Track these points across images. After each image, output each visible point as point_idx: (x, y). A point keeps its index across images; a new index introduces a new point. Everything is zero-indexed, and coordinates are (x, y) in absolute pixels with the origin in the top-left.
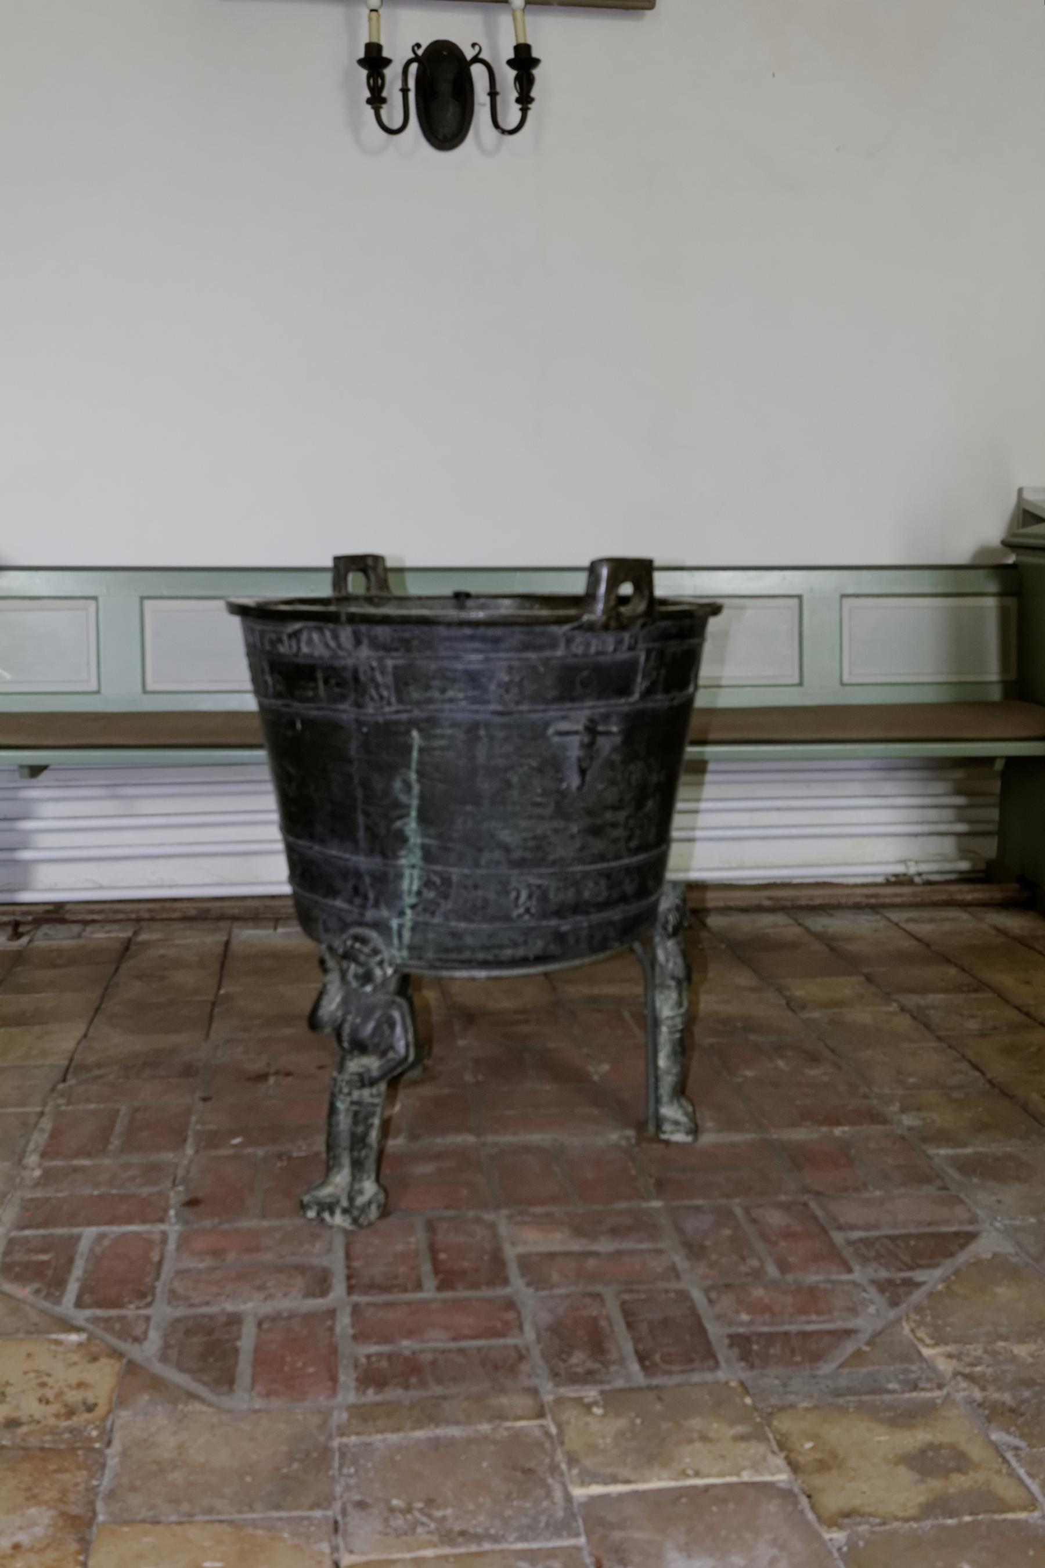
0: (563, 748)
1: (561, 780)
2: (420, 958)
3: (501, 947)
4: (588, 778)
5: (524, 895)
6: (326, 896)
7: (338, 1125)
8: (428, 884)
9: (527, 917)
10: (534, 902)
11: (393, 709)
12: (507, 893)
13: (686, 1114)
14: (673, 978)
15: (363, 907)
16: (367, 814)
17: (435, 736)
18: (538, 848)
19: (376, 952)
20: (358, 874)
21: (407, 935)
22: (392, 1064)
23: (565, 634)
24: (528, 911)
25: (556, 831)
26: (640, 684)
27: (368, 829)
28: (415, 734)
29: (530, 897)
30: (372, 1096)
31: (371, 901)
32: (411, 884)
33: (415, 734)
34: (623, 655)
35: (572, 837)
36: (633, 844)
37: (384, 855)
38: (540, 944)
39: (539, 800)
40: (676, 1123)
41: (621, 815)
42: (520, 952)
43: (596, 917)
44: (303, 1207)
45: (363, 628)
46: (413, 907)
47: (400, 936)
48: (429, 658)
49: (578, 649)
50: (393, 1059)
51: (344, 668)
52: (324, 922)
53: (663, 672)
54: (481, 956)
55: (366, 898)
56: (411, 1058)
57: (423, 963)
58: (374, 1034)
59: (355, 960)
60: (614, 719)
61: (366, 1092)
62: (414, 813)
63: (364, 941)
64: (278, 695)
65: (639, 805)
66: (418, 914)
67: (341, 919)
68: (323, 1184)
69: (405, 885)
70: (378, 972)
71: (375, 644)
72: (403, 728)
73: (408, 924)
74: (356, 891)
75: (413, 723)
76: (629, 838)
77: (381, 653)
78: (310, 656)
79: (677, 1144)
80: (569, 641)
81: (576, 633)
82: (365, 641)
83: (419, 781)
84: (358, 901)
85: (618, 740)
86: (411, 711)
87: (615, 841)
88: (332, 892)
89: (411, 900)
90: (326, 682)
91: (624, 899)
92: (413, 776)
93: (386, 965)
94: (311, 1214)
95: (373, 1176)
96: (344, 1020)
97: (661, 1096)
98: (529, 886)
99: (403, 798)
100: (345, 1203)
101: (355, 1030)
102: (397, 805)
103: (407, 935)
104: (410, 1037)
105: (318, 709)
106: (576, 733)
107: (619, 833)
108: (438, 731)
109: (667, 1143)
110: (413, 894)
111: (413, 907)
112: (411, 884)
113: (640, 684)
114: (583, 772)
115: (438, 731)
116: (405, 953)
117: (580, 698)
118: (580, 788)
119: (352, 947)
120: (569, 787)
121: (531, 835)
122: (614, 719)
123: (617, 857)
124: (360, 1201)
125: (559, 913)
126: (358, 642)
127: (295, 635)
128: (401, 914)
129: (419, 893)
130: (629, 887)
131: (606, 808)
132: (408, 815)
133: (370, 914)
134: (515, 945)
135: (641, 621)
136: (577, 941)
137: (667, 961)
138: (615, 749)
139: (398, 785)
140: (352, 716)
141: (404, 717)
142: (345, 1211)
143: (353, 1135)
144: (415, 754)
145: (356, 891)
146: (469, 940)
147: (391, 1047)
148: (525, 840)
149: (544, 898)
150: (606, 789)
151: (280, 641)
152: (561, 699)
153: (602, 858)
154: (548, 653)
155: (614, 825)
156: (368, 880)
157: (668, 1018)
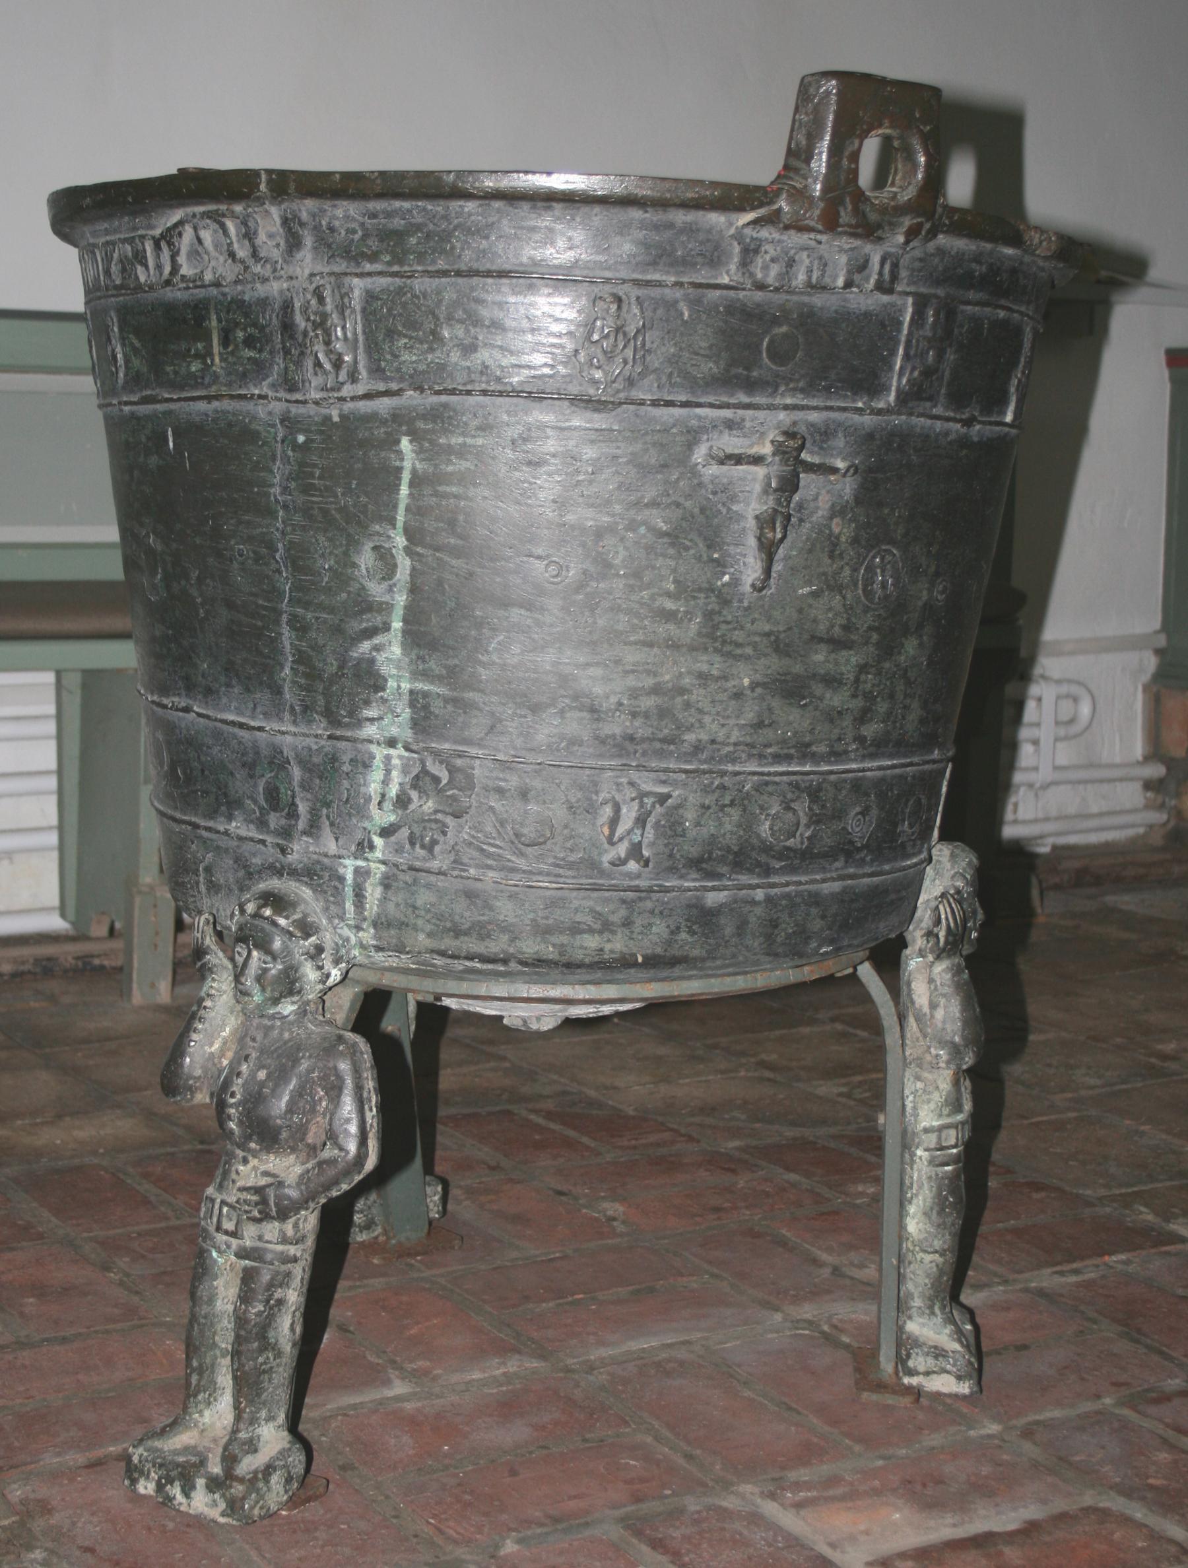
0: (727, 492)
1: (720, 565)
2: (400, 949)
3: (576, 930)
4: (777, 567)
5: (629, 815)
6: (212, 814)
7: (211, 1300)
8: (421, 780)
9: (633, 866)
10: (650, 834)
11: (361, 389)
12: (591, 809)
13: (959, 1334)
14: (942, 1043)
15: (286, 833)
16: (300, 628)
17: (449, 450)
18: (664, 713)
19: (306, 928)
20: (278, 762)
21: (373, 893)
22: (331, 1172)
23: (739, 237)
24: (635, 851)
25: (703, 677)
26: (897, 378)
27: (301, 658)
28: (405, 444)
29: (641, 822)
30: (284, 1240)
31: (301, 824)
32: (386, 782)
33: (405, 444)
34: (865, 299)
35: (738, 695)
36: (871, 730)
37: (332, 718)
38: (660, 929)
39: (670, 605)
40: (938, 1353)
41: (847, 663)
42: (617, 945)
43: (788, 884)
44: (133, 1472)
45: (306, 207)
46: (386, 832)
47: (359, 895)
48: (445, 273)
49: (767, 270)
50: (332, 1162)
51: (264, 302)
52: (208, 870)
53: (951, 356)
54: (530, 947)
55: (293, 814)
56: (371, 1163)
57: (405, 960)
58: (290, 1110)
59: (264, 945)
60: (840, 442)
61: (271, 1230)
62: (397, 625)
63: (279, 902)
64: (135, 380)
65: (888, 649)
66: (399, 850)
67: (240, 861)
68: (174, 1426)
69: (374, 779)
70: (310, 973)
71: (326, 244)
72: (380, 432)
73: (378, 870)
74: (273, 796)
75: (401, 421)
76: (863, 717)
77: (340, 266)
78: (197, 282)
79: (938, 1395)
80: (750, 251)
81: (764, 233)
82: (308, 241)
83: (408, 551)
84: (275, 820)
85: (847, 487)
86: (398, 393)
87: (833, 716)
88: (227, 804)
89: (384, 817)
90: (225, 341)
91: (846, 850)
92: (400, 541)
93: (327, 958)
94: (146, 1487)
95: (281, 1417)
96: (235, 1072)
97: (910, 1296)
98: (642, 795)
99: (376, 590)
100: (216, 1469)
101: (255, 1099)
102: (365, 605)
103: (373, 893)
104: (371, 1115)
105: (209, 398)
106: (757, 460)
107: (836, 699)
108: (455, 440)
109: (917, 1393)
110: (388, 805)
111: (386, 832)
112: (386, 782)
113: (897, 378)
114: (768, 550)
115: (455, 440)
116: (368, 936)
117: (770, 385)
118: (759, 588)
119: (257, 915)
120: (735, 582)
121: (649, 682)
122: (840, 442)
123: (837, 755)
124: (248, 1464)
125: (702, 864)
126: (293, 244)
127: (169, 237)
128: (364, 846)
129: (402, 801)
130: (858, 826)
131: (815, 639)
132: (387, 628)
133: (300, 850)
134: (607, 927)
135: (907, 221)
136: (741, 927)
137: (933, 1006)
138: (838, 511)
139: (365, 559)
140: (277, 407)
141: (384, 405)
142: (214, 1484)
143: (240, 1320)
144: (404, 490)
145: (273, 796)
146: (506, 910)
147: (332, 1136)
148: (634, 693)
149: (672, 828)
150: (815, 595)
151: (140, 258)
152: (725, 381)
153: (804, 752)
154: (702, 275)
155: (832, 681)
156: (296, 772)
157: (926, 1131)
